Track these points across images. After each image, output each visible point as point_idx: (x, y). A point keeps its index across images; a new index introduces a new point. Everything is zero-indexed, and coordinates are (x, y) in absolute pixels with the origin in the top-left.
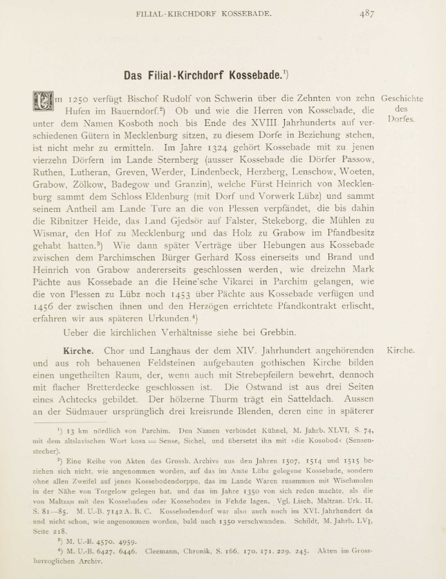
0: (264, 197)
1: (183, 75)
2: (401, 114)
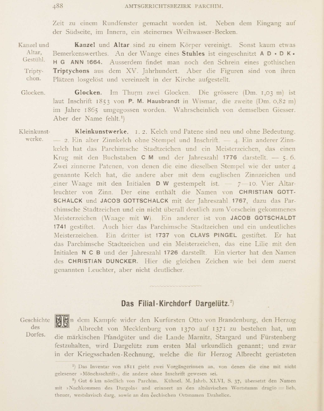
0: (230, 210)
1: (163, 303)
2: (35, 331)
